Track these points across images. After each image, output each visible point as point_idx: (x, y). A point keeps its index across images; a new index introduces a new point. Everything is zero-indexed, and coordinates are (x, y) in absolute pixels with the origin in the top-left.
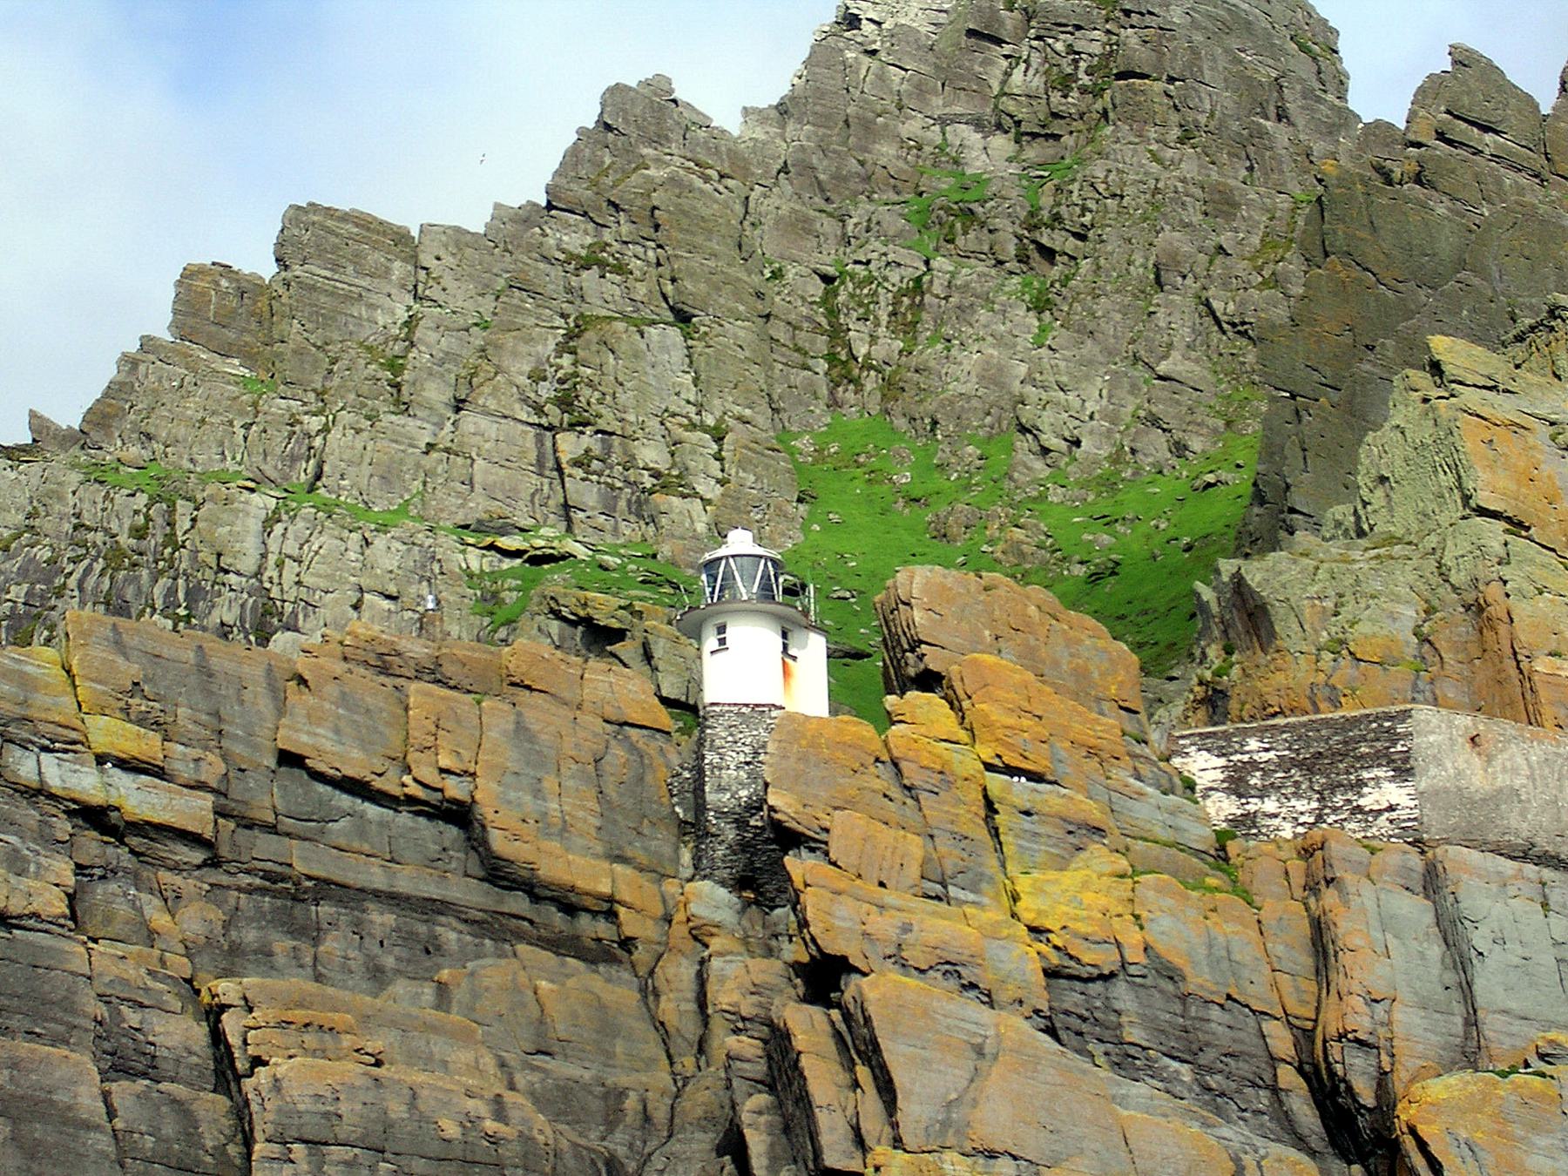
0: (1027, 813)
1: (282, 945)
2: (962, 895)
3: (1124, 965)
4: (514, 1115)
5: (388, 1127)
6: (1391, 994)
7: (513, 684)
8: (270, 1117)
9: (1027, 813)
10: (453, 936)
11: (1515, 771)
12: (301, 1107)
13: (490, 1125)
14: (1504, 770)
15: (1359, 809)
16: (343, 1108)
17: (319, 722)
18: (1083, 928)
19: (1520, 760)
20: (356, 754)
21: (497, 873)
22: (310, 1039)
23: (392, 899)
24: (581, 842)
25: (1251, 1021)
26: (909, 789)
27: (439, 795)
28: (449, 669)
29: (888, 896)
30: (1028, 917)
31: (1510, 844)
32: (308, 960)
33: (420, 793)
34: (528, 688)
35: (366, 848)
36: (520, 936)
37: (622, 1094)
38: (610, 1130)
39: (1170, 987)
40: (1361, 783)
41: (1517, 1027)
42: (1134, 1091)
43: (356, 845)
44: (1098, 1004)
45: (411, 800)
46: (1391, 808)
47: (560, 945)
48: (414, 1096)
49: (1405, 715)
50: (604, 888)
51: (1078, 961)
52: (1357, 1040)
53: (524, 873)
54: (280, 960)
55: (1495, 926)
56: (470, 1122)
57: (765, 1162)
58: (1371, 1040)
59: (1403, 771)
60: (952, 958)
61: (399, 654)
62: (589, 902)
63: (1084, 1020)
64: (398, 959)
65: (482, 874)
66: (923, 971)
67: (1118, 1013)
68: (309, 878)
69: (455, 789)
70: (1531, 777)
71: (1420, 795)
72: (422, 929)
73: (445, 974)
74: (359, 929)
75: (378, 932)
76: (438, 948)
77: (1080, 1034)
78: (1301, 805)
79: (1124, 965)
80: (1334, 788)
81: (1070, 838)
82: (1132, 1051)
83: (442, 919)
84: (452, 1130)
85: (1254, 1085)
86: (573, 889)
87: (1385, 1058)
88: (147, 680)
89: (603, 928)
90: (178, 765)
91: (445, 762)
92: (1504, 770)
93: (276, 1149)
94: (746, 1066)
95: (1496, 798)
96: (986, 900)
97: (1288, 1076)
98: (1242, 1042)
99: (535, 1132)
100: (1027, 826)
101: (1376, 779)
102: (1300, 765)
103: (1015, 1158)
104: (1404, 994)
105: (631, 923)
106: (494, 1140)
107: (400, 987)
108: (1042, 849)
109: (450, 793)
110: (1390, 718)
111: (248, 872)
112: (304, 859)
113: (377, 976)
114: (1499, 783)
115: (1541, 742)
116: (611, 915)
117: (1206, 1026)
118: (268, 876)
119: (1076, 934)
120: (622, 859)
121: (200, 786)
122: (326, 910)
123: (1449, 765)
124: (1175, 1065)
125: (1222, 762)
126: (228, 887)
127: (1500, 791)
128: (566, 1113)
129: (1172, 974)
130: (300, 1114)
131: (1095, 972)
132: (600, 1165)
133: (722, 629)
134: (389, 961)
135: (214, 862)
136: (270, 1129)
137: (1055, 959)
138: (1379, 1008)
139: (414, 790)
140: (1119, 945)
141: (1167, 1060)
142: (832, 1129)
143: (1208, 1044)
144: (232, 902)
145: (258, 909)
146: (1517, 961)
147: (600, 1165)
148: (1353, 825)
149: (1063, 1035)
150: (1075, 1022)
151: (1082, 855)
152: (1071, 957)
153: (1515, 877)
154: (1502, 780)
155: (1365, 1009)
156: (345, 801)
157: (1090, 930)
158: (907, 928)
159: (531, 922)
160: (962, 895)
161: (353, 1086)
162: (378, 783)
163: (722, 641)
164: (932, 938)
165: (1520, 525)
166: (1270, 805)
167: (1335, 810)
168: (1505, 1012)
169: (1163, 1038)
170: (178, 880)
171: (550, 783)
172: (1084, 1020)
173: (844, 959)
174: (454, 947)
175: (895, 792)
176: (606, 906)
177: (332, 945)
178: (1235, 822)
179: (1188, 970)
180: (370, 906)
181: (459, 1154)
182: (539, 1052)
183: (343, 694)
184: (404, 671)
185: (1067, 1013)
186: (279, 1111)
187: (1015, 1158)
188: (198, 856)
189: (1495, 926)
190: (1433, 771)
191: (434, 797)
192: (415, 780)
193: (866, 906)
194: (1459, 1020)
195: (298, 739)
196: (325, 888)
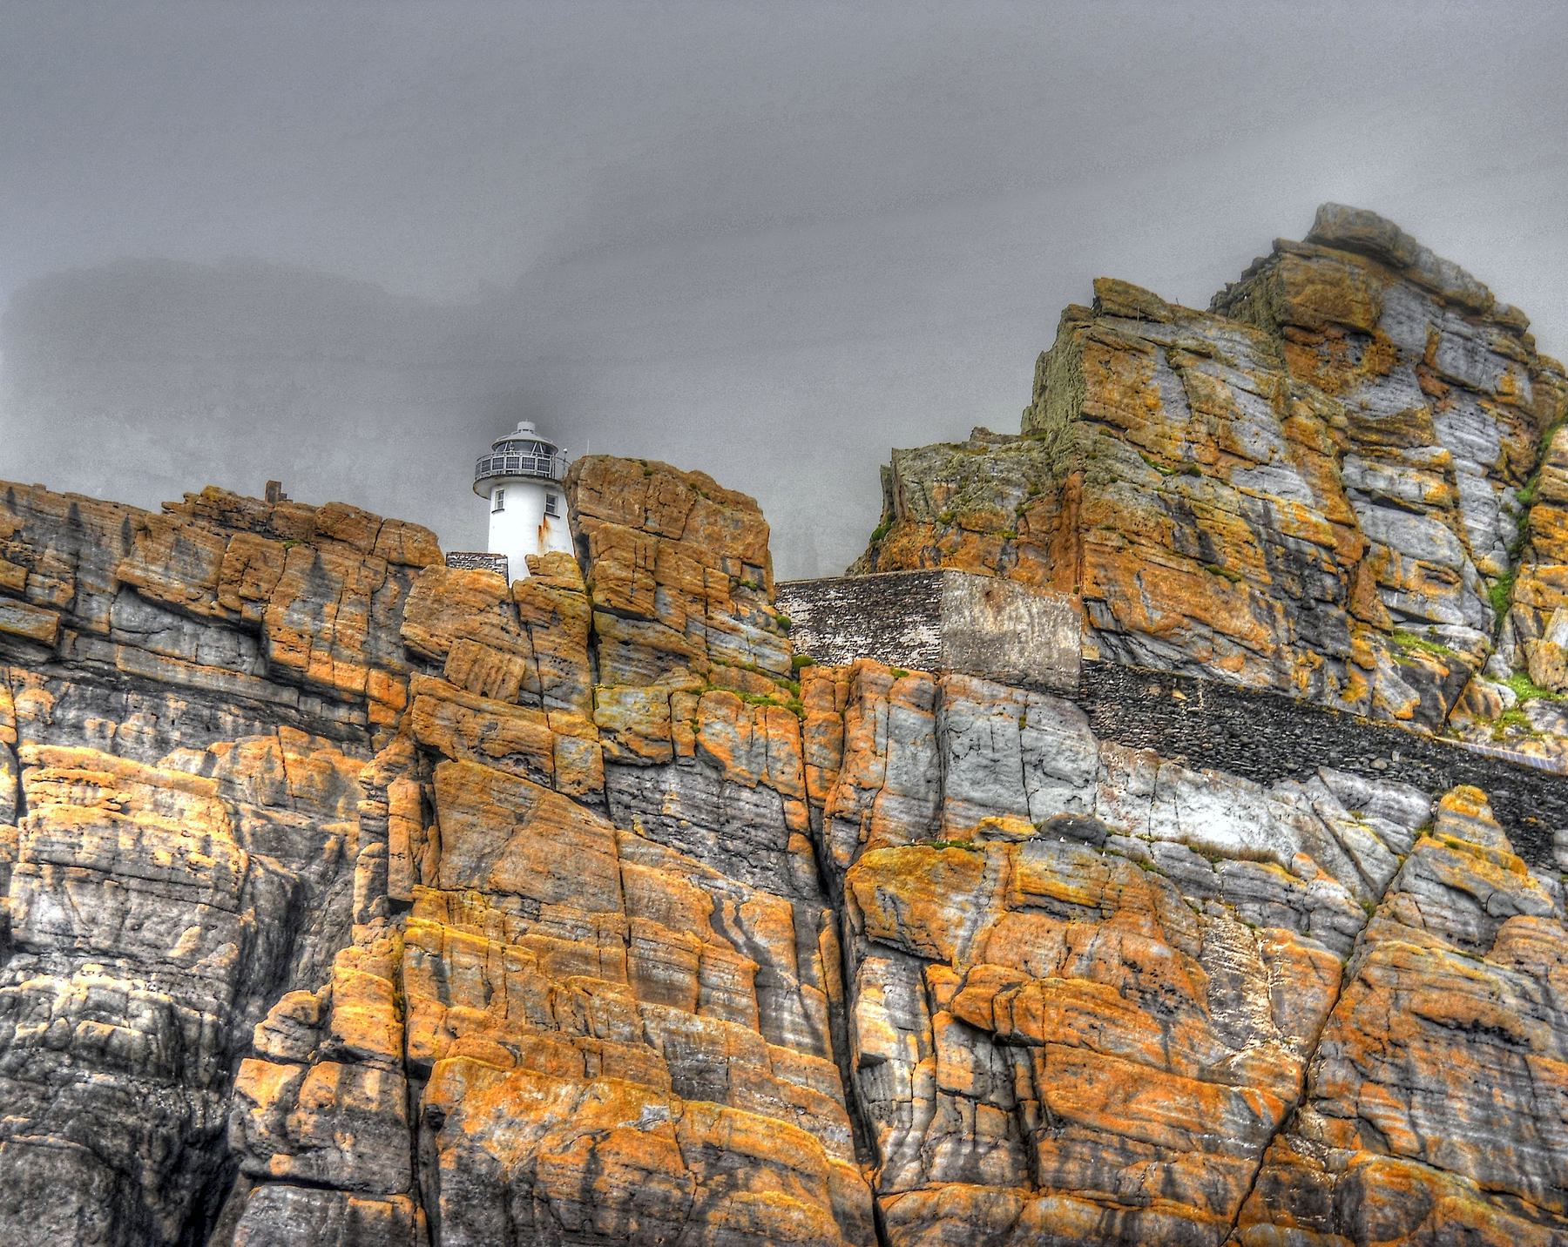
0: (626, 643)
1: (91, 721)
2: (554, 703)
3: (675, 757)
4: (216, 849)
5: (116, 856)
6: (879, 784)
7: (319, 535)
8: (30, 845)
9: (626, 643)
10: (230, 718)
11: (1019, 619)
12: (54, 839)
13: (194, 857)
14: (1010, 618)
15: (900, 645)
16: (85, 840)
17: (154, 561)
18: (643, 729)
19: (1023, 611)
20: (177, 585)
21: (277, 675)
22: (77, 791)
23: (180, 688)
24: (347, 652)
25: (777, 802)
26: (526, 623)
27: (235, 617)
28: (278, 523)
29: (486, 704)
30: (600, 720)
31: (1008, 676)
32: (110, 733)
33: (224, 614)
34: (331, 538)
35: (177, 652)
36: (285, 720)
37: (325, 836)
38: (309, 864)
39: (714, 775)
40: (903, 625)
41: (974, 811)
42: (652, 850)
43: (169, 650)
44: (649, 785)
45: (216, 618)
46: (922, 645)
47: (313, 728)
48: (141, 834)
49: (940, 574)
50: (358, 685)
51: (637, 754)
52: (842, 818)
53: (296, 675)
54: (88, 733)
55: (975, 736)
56: (182, 852)
57: (364, 891)
58: (855, 818)
59: (933, 617)
60: (523, 749)
61: (239, 511)
62: (346, 696)
63: (635, 797)
64: (183, 734)
65: (262, 672)
66: (497, 759)
67: (663, 793)
68: (127, 673)
69: (250, 612)
70: (1031, 624)
71: (943, 636)
72: (206, 712)
73: (214, 746)
74: (157, 714)
75: (172, 714)
76: (217, 728)
77: (628, 807)
78: (860, 640)
79: (675, 757)
80: (883, 629)
81: (659, 663)
82: (667, 821)
83: (225, 707)
84: (164, 858)
85: (768, 849)
86: (333, 686)
87: (863, 832)
88: (27, 528)
89: (356, 717)
90: (38, 591)
91: (243, 591)
92: (1010, 618)
93: (31, 867)
94: (372, 822)
95: (999, 640)
96: (574, 708)
97: (797, 841)
98: (764, 816)
99: (230, 864)
100: (623, 652)
101: (914, 622)
102: (862, 610)
103: (522, 897)
104: (891, 784)
105: (378, 715)
106: (196, 868)
107: (178, 755)
108: (629, 671)
109: (245, 614)
110: (929, 578)
111: (83, 669)
112: (127, 660)
113: (162, 745)
114: (1005, 628)
115: (1042, 598)
116: (363, 706)
117: (736, 804)
118: (99, 672)
119: (637, 734)
120: (378, 665)
121: (51, 606)
122: (132, 698)
123: (967, 613)
124: (704, 832)
125: (810, 606)
126: (168, 686)
127: (1005, 634)
128: (276, 849)
129: (717, 765)
130: (52, 844)
131: (649, 762)
132: (288, 887)
133: (500, 495)
134: (175, 735)
135: (56, 661)
136: (29, 853)
137: (616, 751)
138: (866, 795)
139: (219, 612)
140: (673, 742)
141: (696, 829)
142: (397, 871)
143: (734, 818)
144: (63, 689)
145: (82, 697)
146: (985, 762)
147: (288, 887)
148: (895, 657)
149: (614, 808)
150: (626, 798)
151: (666, 675)
152: (631, 751)
153: (1006, 699)
154: (1008, 626)
155: (855, 796)
156: (167, 620)
157: (650, 730)
158: (492, 727)
159: (297, 710)
160: (554, 703)
161: (95, 826)
162: (192, 607)
163: (500, 504)
164: (509, 735)
165: (1118, 427)
166: (839, 640)
167: (883, 645)
168: (968, 800)
169: (695, 813)
170: (24, 673)
171: (329, 608)
172: (635, 797)
173: (436, 748)
174: (229, 727)
175: (513, 627)
176: (359, 700)
177: (133, 723)
178: (814, 651)
179: (729, 763)
180: (170, 695)
181: (166, 876)
182: (274, 805)
183: (178, 541)
184: (241, 524)
185: (620, 791)
186: (38, 840)
187: (522, 897)
188: (42, 657)
189: (975, 736)
190: (955, 617)
191: (235, 617)
192: (222, 605)
193: (463, 710)
194: (931, 805)
195: (135, 572)
196: (141, 684)
